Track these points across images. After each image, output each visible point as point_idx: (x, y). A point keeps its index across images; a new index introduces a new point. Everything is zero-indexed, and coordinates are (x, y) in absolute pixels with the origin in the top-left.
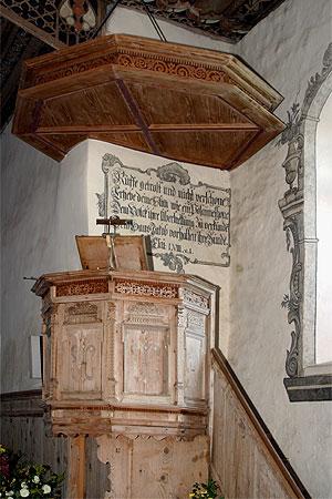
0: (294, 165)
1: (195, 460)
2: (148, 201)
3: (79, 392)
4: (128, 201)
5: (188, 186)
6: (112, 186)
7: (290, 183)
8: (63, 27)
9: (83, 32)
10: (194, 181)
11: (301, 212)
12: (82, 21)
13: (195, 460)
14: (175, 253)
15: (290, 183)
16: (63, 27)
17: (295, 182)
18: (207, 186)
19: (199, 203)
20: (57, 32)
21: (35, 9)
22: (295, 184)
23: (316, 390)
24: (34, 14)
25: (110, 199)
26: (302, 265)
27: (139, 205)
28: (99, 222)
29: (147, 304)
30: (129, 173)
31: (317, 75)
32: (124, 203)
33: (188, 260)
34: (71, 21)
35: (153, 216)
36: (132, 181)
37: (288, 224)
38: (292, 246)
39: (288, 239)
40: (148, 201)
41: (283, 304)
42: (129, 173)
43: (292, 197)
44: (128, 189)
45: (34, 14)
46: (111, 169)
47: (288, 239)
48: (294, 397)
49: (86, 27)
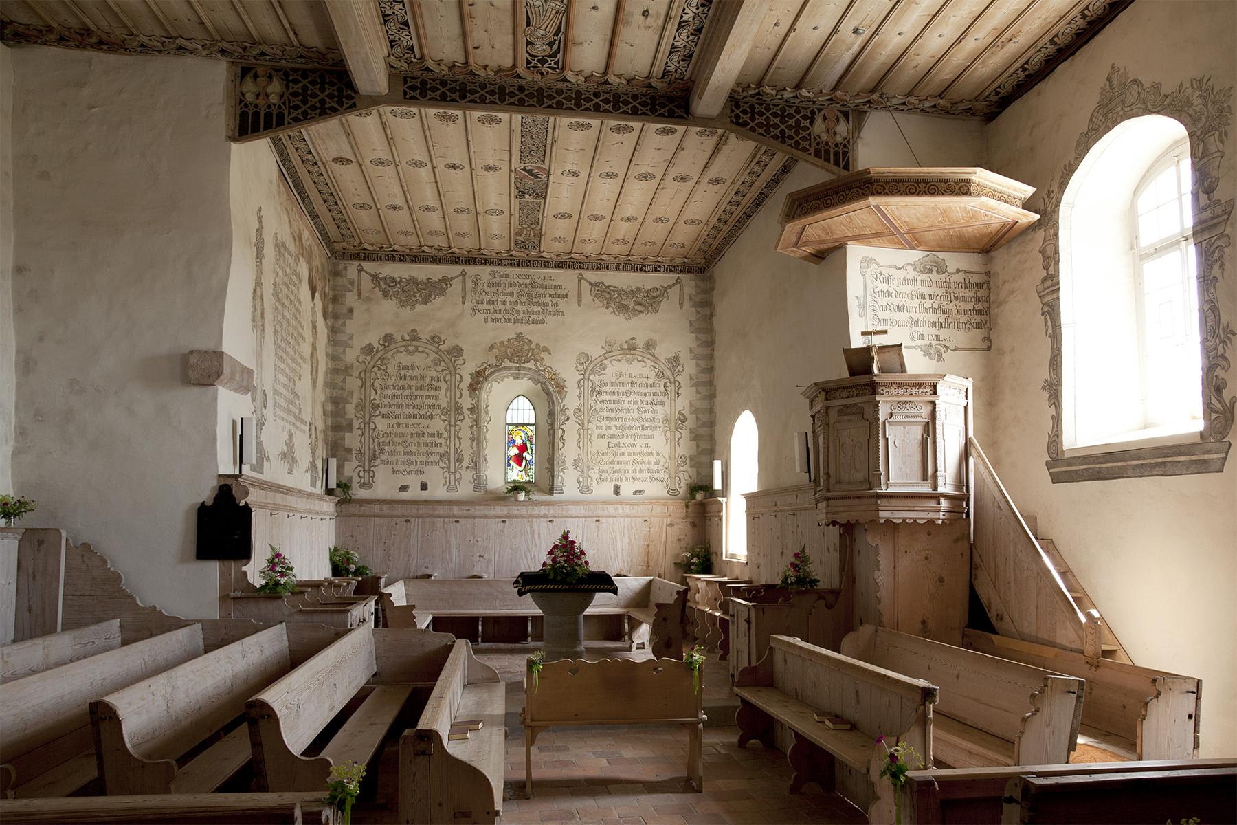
0: (1049, 252)
1: (956, 541)
2: (905, 295)
3: (849, 483)
4: (886, 299)
5: (945, 275)
6: (870, 286)
7: (1047, 269)
8: (818, 144)
9: (836, 145)
10: (951, 269)
11: (1058, 298)
12: (835, 134)
13: (956, 541)
14: (934, 343)
15: (1047, 269)
16: (818, 144)
17: (1051, 269)
18: (965, 272)
19: (957, 291)
20: (812, 150)
21: (791, 133)
22: (1051, 270)
23: (1076, 471)
24: (791, 137)
25: (869, 299)
26: (1059, 349)
27: (897, 301)
28: (864, 334)
29: (309, 511)
30: (885, 271)
31: (1070, 164)
32: (883, 301)
33: (947, 348)
34: (824, 137)
35: (910, 309)
36: (889, 279)
37: (1046, 309)
38: (1050, 331)
39: (1046, 324)
40: (905, 295)
41: (1043, 387)
42: (885, 271)
43: (1049, 283)
44: (885, 287)
45: (791, 137)
46: (868, 270)
47: (1046, 324)
48: (1056, 479)
49: (839, 139)
